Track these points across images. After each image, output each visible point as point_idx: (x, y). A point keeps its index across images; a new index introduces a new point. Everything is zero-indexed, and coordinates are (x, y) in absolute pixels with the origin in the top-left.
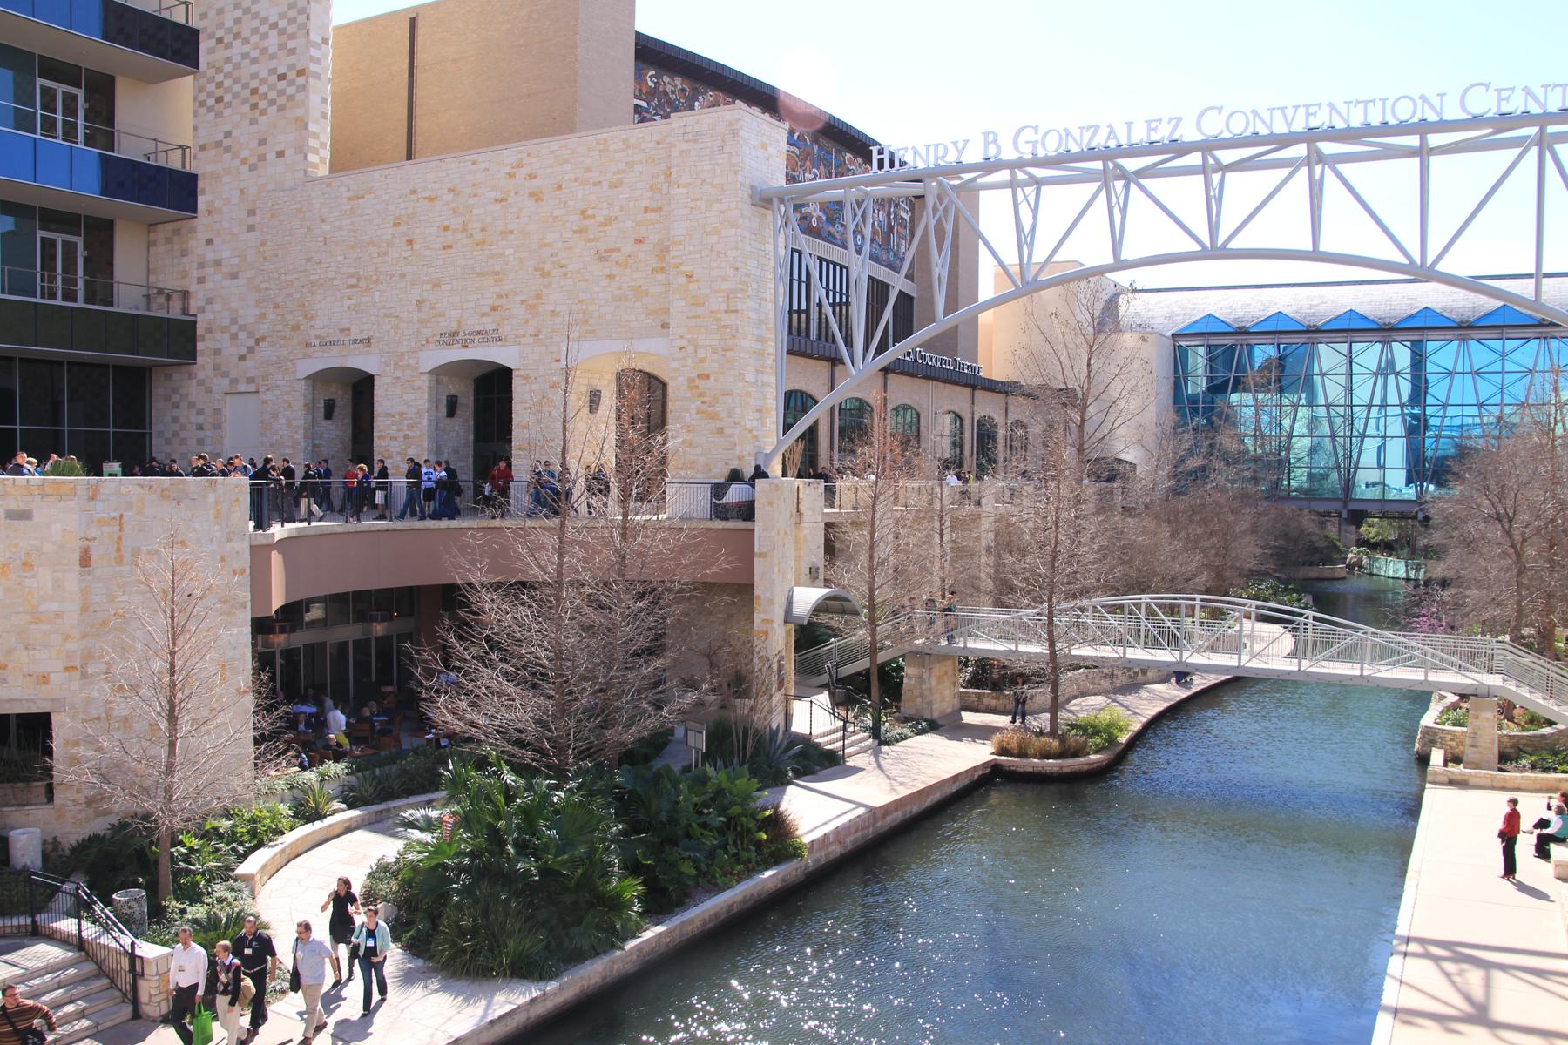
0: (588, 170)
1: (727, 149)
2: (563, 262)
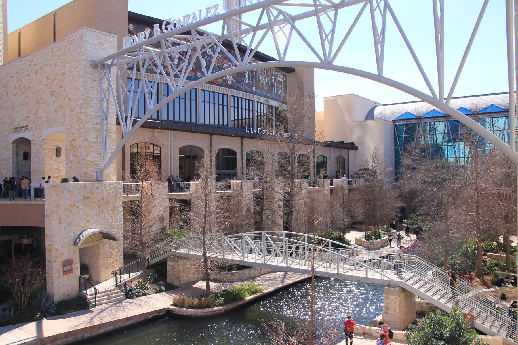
0: (49, 60)
1: (80, 46)
2: (43, 97)
